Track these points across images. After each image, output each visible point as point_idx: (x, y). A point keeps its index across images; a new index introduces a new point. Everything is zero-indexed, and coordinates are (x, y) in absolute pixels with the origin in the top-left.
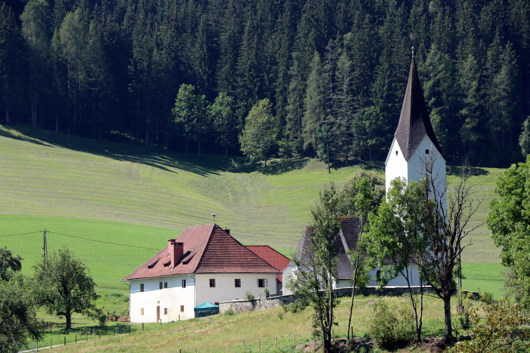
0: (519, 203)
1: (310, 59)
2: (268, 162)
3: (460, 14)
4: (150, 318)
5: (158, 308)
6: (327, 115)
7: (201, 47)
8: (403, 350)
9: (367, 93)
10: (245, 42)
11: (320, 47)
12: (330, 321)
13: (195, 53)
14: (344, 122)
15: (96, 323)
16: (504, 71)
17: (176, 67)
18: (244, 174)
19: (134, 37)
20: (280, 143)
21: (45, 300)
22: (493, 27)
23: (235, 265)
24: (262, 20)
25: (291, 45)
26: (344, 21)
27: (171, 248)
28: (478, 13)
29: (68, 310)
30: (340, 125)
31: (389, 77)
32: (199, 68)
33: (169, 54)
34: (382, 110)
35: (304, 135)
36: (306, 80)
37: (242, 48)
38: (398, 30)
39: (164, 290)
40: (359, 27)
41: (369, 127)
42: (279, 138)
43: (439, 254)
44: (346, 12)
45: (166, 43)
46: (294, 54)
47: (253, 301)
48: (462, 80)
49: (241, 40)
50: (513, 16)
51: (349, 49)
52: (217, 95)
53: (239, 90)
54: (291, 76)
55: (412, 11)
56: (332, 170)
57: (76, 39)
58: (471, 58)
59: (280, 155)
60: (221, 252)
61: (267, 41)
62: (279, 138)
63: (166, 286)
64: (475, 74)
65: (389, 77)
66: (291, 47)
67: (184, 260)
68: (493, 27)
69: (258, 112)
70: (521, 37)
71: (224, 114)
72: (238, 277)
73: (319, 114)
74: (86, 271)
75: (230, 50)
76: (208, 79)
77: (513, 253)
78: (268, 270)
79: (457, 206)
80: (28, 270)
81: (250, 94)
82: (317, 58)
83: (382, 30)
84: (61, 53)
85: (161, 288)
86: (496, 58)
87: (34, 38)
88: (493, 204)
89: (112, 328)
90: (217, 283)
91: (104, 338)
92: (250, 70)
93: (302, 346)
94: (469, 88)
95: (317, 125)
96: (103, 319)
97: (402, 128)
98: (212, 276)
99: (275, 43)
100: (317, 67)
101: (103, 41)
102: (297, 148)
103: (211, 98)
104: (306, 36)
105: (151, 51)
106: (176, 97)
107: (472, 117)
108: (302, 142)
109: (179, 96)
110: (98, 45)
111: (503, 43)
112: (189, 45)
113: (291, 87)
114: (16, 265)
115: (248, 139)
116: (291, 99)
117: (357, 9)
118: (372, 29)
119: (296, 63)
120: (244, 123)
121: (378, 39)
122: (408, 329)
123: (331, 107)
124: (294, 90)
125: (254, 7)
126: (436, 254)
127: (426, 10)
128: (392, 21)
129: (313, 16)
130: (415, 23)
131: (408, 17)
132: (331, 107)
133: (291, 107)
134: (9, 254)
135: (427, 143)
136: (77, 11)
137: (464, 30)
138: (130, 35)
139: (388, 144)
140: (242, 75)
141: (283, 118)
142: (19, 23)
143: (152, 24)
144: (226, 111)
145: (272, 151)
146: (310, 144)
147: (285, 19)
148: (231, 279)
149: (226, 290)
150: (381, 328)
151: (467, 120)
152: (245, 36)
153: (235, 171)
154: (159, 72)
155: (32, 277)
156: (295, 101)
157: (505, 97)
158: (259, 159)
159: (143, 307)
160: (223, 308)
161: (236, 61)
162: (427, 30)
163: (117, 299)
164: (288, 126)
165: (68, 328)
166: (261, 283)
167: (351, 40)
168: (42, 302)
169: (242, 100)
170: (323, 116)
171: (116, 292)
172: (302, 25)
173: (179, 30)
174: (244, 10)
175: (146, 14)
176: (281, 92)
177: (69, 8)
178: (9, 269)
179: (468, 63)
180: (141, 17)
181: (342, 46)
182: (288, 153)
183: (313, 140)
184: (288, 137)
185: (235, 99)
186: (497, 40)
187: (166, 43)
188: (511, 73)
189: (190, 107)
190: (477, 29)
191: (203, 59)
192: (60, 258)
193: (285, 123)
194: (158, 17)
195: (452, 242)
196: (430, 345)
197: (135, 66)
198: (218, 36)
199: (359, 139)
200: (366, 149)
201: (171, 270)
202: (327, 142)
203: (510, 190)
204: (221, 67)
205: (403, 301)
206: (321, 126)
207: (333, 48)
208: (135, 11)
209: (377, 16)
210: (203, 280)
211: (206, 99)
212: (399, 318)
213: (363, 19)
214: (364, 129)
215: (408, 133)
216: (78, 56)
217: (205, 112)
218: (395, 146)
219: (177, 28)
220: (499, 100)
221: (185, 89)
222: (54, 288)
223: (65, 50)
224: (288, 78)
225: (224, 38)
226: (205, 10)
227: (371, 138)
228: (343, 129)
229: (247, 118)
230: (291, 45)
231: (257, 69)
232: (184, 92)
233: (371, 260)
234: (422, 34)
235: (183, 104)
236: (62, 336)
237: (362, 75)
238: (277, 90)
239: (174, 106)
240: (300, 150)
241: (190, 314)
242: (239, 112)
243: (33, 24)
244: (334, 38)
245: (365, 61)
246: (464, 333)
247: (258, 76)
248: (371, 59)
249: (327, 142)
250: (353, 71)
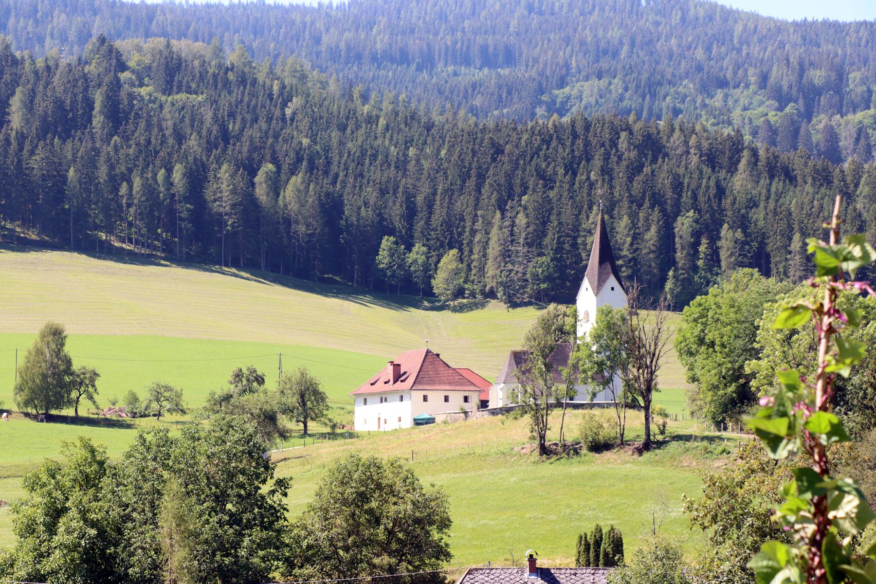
0: (703, 331)
1: (493, 217)
2: (456, 303)
3: (616, 183)
4: (372, 427)
5: (379, 419)
6: (506, 263)
7: (401, 206)
8: (597, 455)
9: (540, 245)
10: (438, 203)
11: (501, 206)
12: (545, 428)
13: (395, 211)
14: (520, 270)
15: (328, 430)
16: (653, 229)
17: (380, 222)
18: (435, 312)
19: (345, 197)
20: (466, 286)
21: (287, 410)
22: (644, 193)
23: (445, 384)
24: (452, 184)
25: (476, 205)
26: (521, 186)
27: (391, 368)
28: (631, 182)
29: (305, 418)
30: (517, 272)
31: (558, 233)
32: (399, 224)
33: (374, 211)
34: (552, 260)
35: (486, 280)
36: (488, 234)
37: (435, 207)
38: (566, 194)
39: (384, 404)
40: (534, 191)
41: (542, 273)
42: (465, 282)
43: (641, 371)
44: (522, 179)
45: (372, 202)
46: (479, 213)
47: (466, 413)
48: (618, 237)
49: (435, 201)
50: (660, 186)
51: (525, 208)
52: (414, 246)
53: (432, 242)
54: (477, 231)
55: (577, 179)
56: (510, 309)
57: (298, 197)
58: (626, 218)
59: (467, 296)
60: (433, 370)
61: (456, 201)
62: (465, 282)
63: (386, 400)
64: (630, 230)
65: (558, 233)
66: (476, 207)
67: (402, 378)
68: (644, 193)
69: (449, 260)
70: (666, 203)
71: (420, 262)
72: (447, 393)
73: (500, 262)
74: (320, 386)
75: (425, 208)
76: (406, 233)
77: (698, 372)
78: (472, 388)
79: (656, 330)
80: (271, 385)
81: (442, 245)
82: (498, 215)
83: (552, 194)
84: (286, 209)
85: (382, 402)
86: (647, 219)
87: (265, 197)
88: (680, 330)
89: (342, 435)
90: (429, 398)
91: (336, 442)
92: (442, 225)
93: (520, 448)
94: (624, 243)
95: (498, 272)
96: (334, 426)
97: (592, 269)
98: (425, 393)
99: (463, 203)
100: (498, 224)
101: (320, 200)
102: (481, 290)
103: (409, 248)
104: (489, 198)
105: (359, 208)
106: (379, 247)
107: (627, 267)
108: (485, 286)
109: (382, 246)
110: (317, 202)
111: (652, 207)
112: (391, 204)
113: (476, 239)
114: (260, 380)
115: (439, 283)
116: (476, 249)
117: (532, 176)
118: (544, 192)
119: (480, 220)
120: (436, 269)
121: (550, 201)
122: (613, 435)
123: (510, 256)
124: (479, 242)
125: (445, 173)
126: (638, 370)
127: (588, 178)
128: (561, 187)
129: (495, 181)
130: (580, 189)
131: (574, 184)
132: (510, 256)
133: (476, 256)
134: (255, 371)
135: (612, 281)
136: (300, 175)
137: (620, 195)
138: (342, 195)
139: (582, 279)
140: (435, 230)
141: (469, 266)
142: (253, 185)
143: (361, 187)
144: (421, 259)
145: (459, 293)
146: (492, 287)
147: (471, 183)
148: (442, 395)
149: (436, 404)
150: (589, 433)
151: (623, 269)
152: (438, 198)
153: (427, 309)
154: (365, 226)
155: (275, 390)
156: (479, 251)
157: (654, 252)
158: (447, 301)
159: (366, 418)
160: (439, 419)
161: (430, 217)
162: (589, 195)
163: (342, 412)
164: (474, 272)
165: (305, 433)
166: (466, 399)
167: (528, 202)
168: (284, 412)
169: (434, 251)
170: (503, 264)
171: (342, 406)
172: (486, 189)
173: (383, 192)
174: (437, 176)
175: (356, 179)
176: (468, 244)
177: (293, 172)
178: (255, 384)
179: (623, 224)
180: (351, 180)
181: (520, 205)
182: (473, 295)
183: (494, 284)
184: (473, 282)
185: (429, 249)
186: (647, 204)
187: (372, 202)
188: (658, 232)
189: (392, 255)
190: (630, 196)
191: (402, 216)
192: (299, 374)
193: (471, 270)
194: (365, 181)
195: (652, 362)
196: (632, 447)
197: (346, 221)
198: (415, 197)
199: (534, 284)
200: (539, 292)
201: (390, 386)
202: (505, 286)
203: (695, 320)
204: (417, 223)
205: (612, 412)
206: (501, 272)
207: (512, 208)
208: (346, 176)
209: (548, 182)
210: (418, 395)
211: (405, 249)
212: (605, 425)
213: (537, 185)
214: (538, 275)
215: (596, 273)
216: (300, 212)
217: (404, 259)
218: (586, 284)
219: (381, 190)
220: (649, 253)
221: (388, 240)
222: (294, 400)
223: (289, 207)
224: (473, 232)
225: (420, 199)
226: (404, 175)
227: (544, 282)
228: (520, 275)
229: (439, 265)
230: (476, 205)
231: (448, 224)
232: (386, 242)
233: (583, 375)
234: (585, 198)
235: (385, 252)
236: (302, 440)
237: (535, 230)
238: (465, 242)
239: (378, 255)
240: (483, 292)
241: (408, 423)
242: (432, 261)
243: (264, 186)
244: (513, 200)
245: (538, 219)
246: (660, 438)
247: (448, 230)
248: (544, 217)
249: (505, 286)
250: (528, 227)
